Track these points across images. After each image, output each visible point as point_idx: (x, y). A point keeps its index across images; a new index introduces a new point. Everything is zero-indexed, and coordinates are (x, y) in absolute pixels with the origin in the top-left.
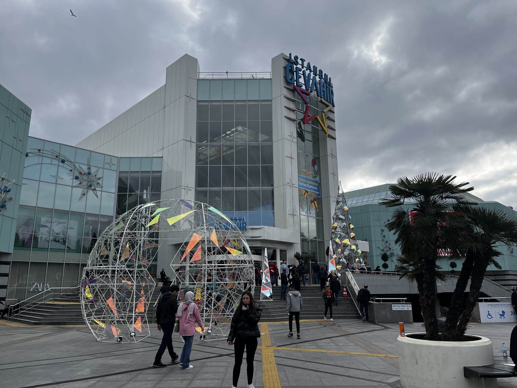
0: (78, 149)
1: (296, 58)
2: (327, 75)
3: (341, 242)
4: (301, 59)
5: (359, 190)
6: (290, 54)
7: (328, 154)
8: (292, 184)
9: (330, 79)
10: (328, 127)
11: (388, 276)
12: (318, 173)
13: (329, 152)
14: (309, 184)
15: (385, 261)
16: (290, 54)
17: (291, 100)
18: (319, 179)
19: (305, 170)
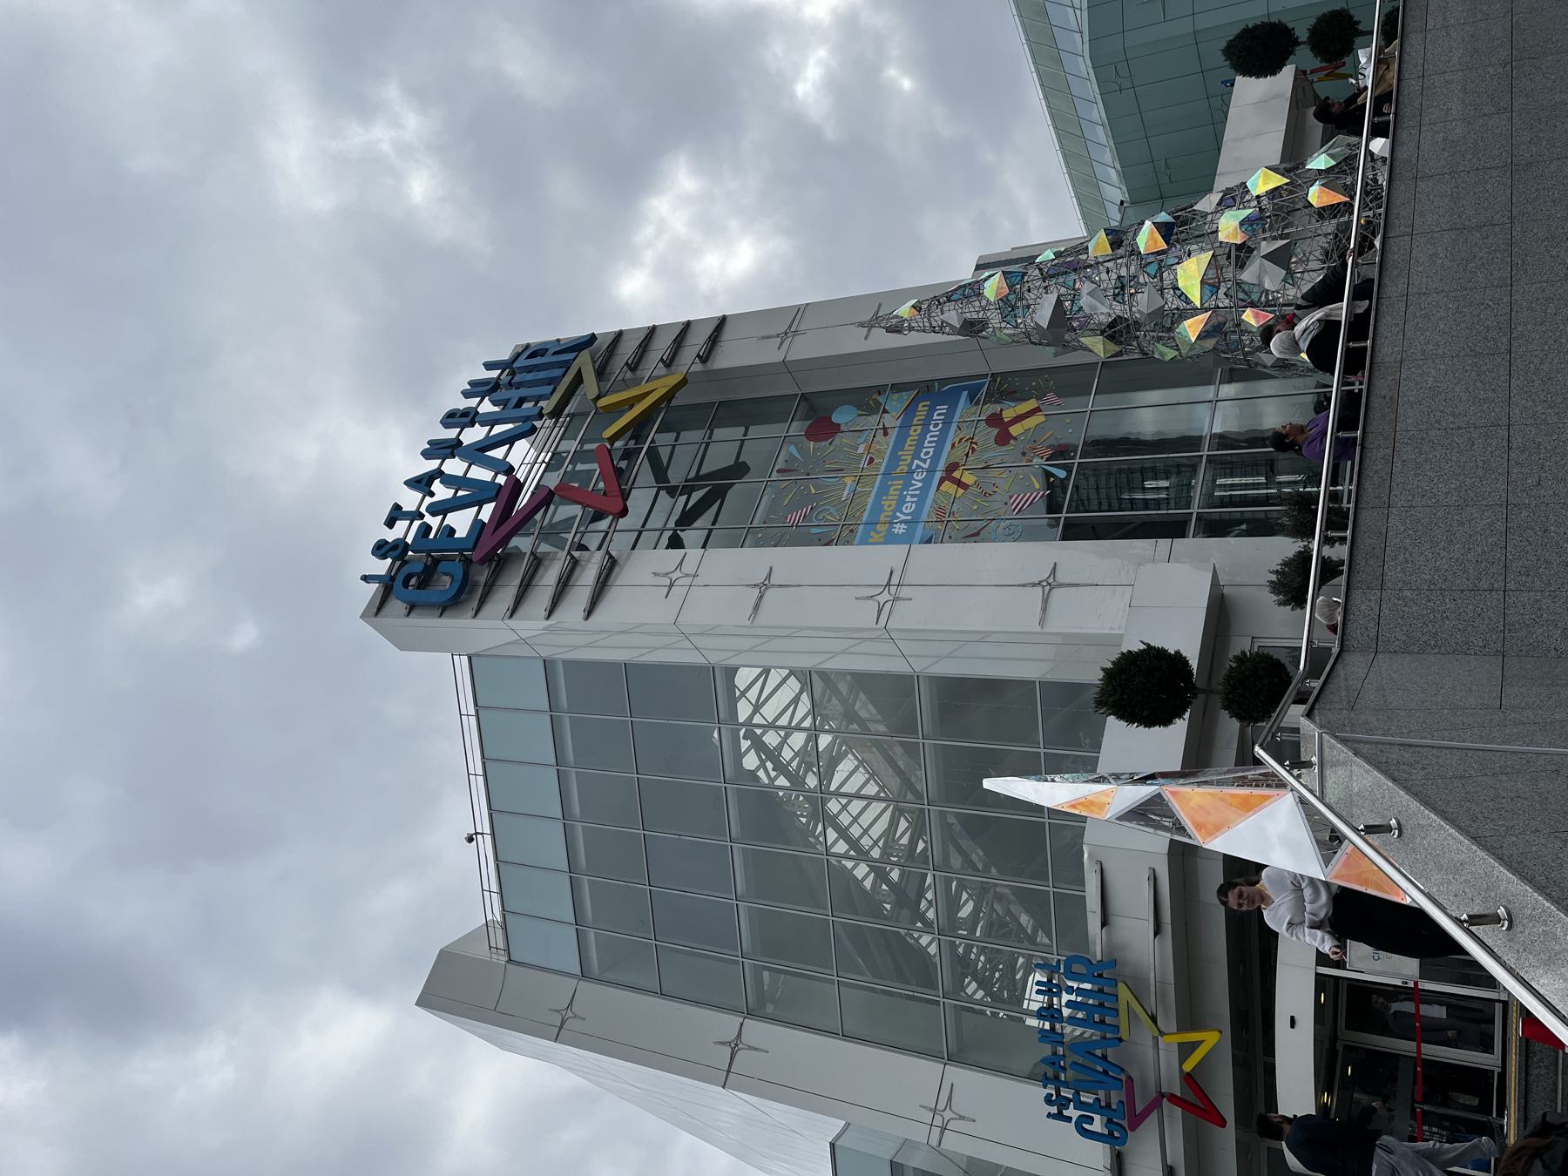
0: (942, 1142)
1: (381, 549)
2: (470, 383)
3: (1195, 312)
4: (390, 523)
5: (1046, 97)
6: (366, 578)
7: (781, 359)
8: (888, 584)
9: (489, 366)
10: (669, 363)
11: (1414, 40)
12: (867, 400)
13: (770, 355)
14: (916, 456)
15: (1296, 43)
16: (366, 578)
17: (532, 578)
18: (896, 396)
19: (846, 484)
